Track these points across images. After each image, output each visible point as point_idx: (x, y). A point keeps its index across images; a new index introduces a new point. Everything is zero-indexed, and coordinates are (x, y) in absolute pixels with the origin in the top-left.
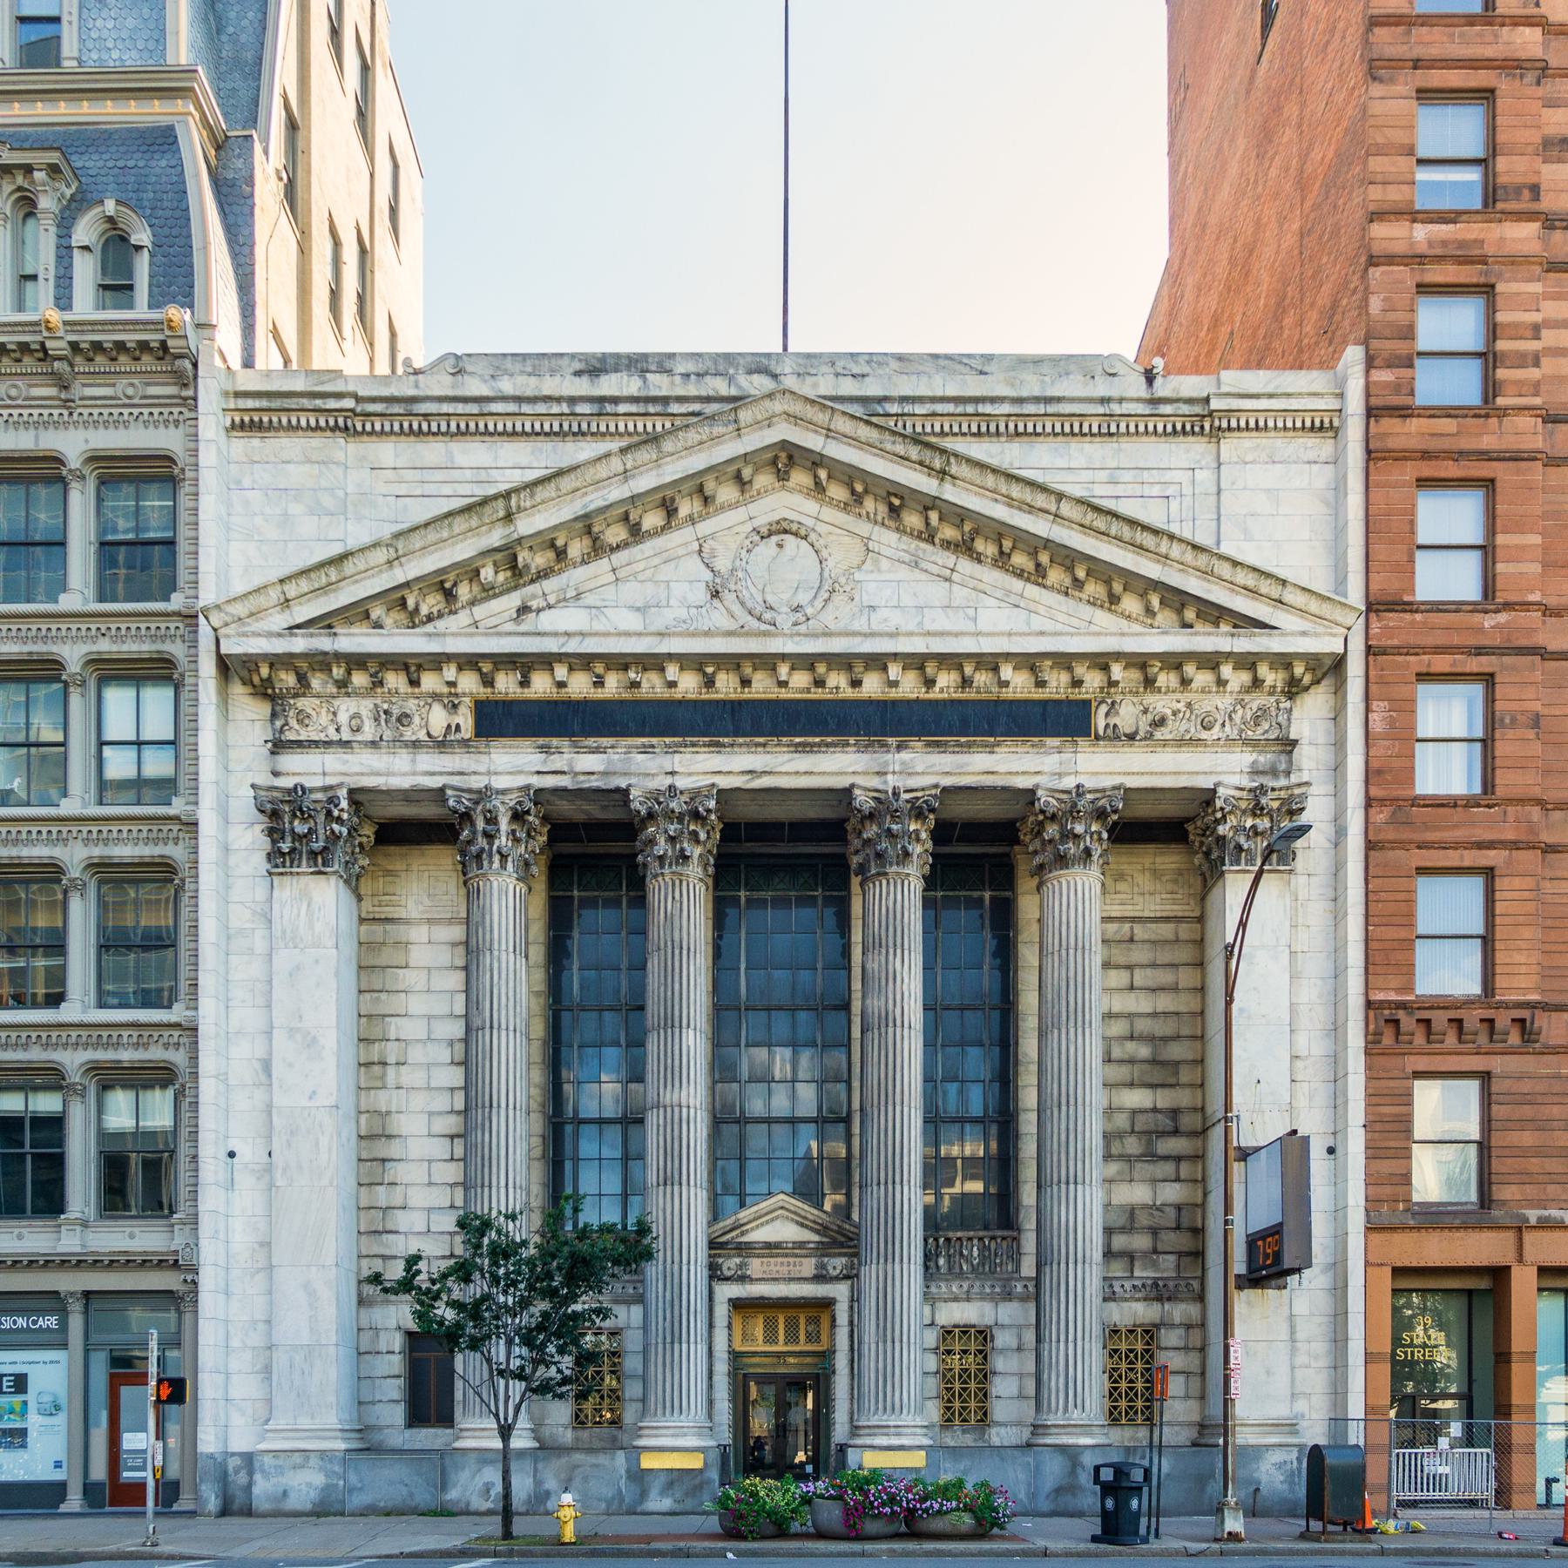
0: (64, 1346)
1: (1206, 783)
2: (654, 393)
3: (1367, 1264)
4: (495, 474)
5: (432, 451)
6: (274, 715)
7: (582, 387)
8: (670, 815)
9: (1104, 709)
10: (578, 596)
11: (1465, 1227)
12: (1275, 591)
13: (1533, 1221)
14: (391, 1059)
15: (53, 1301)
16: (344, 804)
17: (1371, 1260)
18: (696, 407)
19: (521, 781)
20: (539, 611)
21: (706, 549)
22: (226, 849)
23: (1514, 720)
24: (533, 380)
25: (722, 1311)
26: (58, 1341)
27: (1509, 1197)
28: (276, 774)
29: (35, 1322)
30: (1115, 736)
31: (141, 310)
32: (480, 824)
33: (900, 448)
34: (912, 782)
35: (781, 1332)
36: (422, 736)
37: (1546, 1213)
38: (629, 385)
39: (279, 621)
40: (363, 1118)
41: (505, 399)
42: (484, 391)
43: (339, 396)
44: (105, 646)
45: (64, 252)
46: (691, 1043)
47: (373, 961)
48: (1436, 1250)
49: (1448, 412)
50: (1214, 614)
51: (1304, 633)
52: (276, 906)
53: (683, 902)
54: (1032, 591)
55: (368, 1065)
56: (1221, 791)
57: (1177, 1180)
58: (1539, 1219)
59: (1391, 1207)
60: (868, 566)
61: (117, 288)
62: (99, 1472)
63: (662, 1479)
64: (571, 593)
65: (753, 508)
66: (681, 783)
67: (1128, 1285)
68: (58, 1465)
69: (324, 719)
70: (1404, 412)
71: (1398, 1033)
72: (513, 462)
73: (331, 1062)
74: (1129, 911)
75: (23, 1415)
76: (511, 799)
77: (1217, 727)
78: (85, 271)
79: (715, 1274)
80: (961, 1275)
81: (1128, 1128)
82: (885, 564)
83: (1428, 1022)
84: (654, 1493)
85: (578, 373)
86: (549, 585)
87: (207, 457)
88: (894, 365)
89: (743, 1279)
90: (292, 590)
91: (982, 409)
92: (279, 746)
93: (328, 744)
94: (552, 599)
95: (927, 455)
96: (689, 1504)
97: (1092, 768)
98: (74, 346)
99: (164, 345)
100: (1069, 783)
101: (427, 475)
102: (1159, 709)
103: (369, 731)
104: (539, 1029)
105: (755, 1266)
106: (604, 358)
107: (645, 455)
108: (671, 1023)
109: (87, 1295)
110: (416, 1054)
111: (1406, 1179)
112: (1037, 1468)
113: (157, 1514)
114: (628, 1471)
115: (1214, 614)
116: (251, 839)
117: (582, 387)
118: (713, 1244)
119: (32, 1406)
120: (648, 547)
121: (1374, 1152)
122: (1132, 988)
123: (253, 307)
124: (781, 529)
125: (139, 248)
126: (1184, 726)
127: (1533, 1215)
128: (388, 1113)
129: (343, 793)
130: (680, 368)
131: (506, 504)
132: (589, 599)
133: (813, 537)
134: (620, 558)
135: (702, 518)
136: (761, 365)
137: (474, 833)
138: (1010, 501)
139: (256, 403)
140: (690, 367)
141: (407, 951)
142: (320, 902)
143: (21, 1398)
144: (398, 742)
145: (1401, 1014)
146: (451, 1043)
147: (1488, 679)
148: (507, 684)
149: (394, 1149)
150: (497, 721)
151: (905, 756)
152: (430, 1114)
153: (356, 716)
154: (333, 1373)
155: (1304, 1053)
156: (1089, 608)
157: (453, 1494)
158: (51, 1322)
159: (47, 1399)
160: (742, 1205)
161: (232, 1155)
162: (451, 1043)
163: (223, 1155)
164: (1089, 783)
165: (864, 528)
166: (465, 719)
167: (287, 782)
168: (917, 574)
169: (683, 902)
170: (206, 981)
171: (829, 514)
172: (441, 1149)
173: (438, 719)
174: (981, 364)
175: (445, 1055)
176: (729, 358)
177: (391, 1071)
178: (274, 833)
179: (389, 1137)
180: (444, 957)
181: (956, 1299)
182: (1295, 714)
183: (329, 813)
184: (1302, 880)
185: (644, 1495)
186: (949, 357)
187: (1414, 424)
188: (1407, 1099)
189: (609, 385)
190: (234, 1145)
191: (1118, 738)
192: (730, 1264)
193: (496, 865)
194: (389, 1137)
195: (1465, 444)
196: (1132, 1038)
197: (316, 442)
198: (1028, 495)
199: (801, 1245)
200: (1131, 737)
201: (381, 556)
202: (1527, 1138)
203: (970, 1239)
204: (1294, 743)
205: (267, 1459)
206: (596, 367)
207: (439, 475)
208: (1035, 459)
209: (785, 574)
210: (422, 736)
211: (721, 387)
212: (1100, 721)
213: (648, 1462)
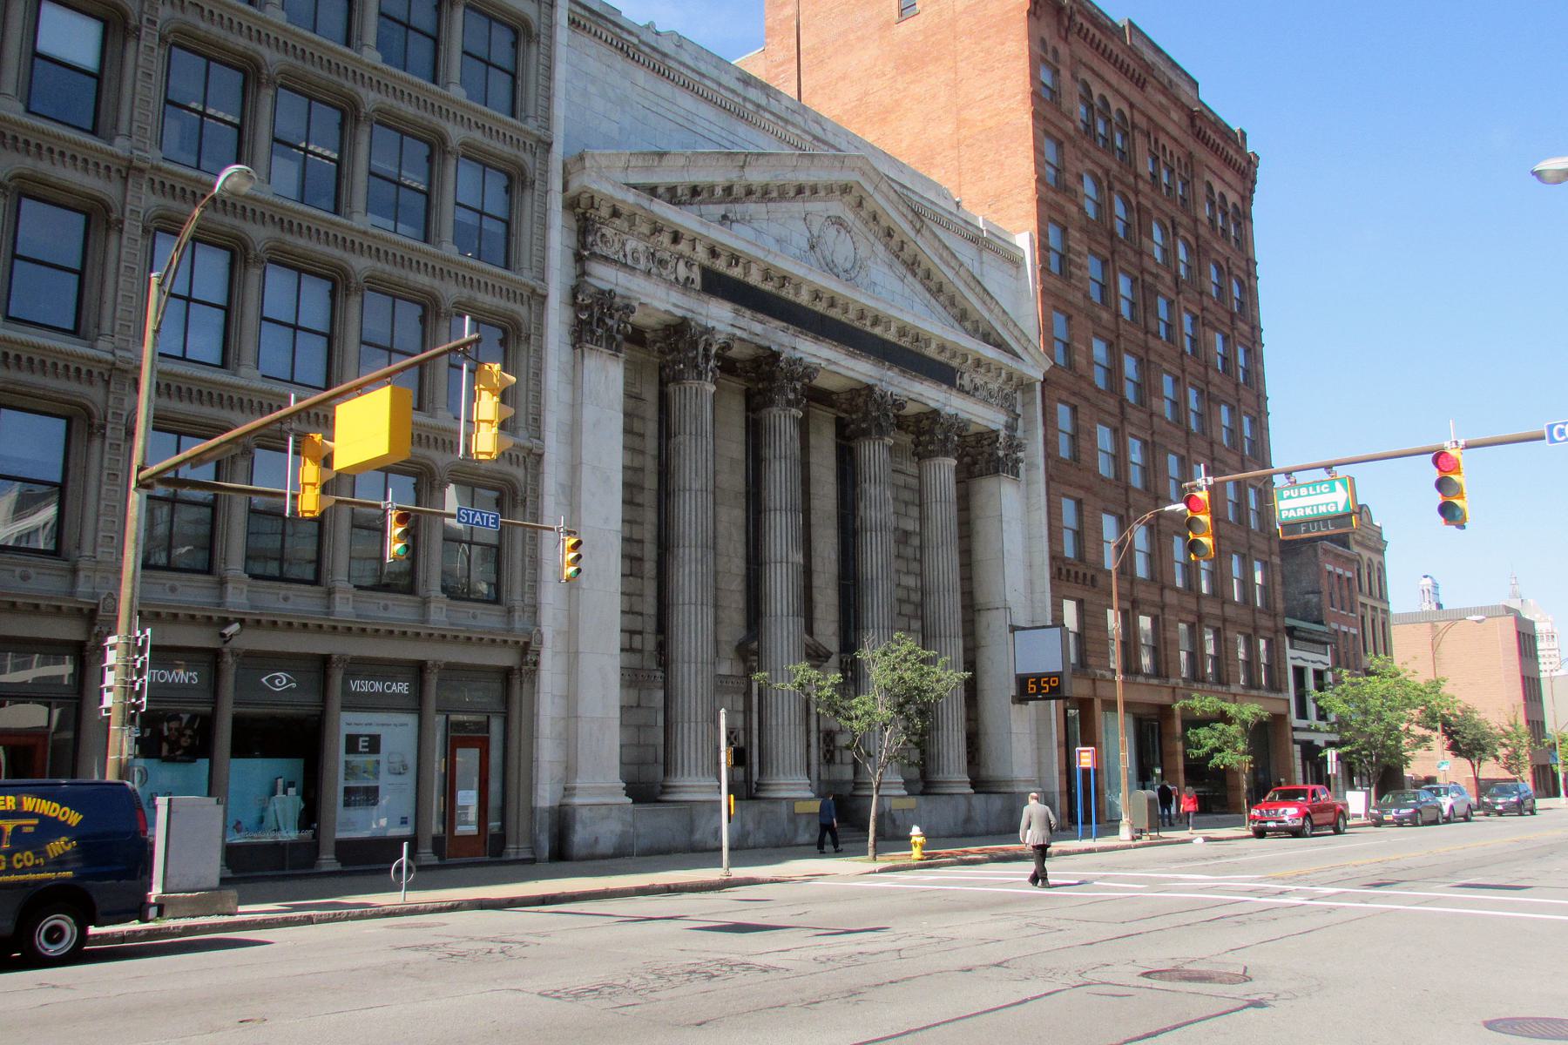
4: (697, 120)
5: (665, 88)
7: (739, 87)
29: (389, 687)
33: (905, 210)
39: (621, 178)
69: (617, 246)
75: (376, 774)
93: (616, 262)
95: (915, 220)
97: (930, 394)
101: (661, 102)
109: (451, 668)
119: (383, 767)
134: (772, 205)
138: (941, 258)
139: (583, 12)
143: (373, 757)
148: (721, 265)
150: (715, 285)
151: (890, 373)
157: (697, 836)
159: (396, 759)
173: (682, 271)
185: (796, 831)
189: (753, 94)
197: (605, 50)
201: (682, 161)
202: (468, 798)
207: (666, 105)
209: (841, 248)
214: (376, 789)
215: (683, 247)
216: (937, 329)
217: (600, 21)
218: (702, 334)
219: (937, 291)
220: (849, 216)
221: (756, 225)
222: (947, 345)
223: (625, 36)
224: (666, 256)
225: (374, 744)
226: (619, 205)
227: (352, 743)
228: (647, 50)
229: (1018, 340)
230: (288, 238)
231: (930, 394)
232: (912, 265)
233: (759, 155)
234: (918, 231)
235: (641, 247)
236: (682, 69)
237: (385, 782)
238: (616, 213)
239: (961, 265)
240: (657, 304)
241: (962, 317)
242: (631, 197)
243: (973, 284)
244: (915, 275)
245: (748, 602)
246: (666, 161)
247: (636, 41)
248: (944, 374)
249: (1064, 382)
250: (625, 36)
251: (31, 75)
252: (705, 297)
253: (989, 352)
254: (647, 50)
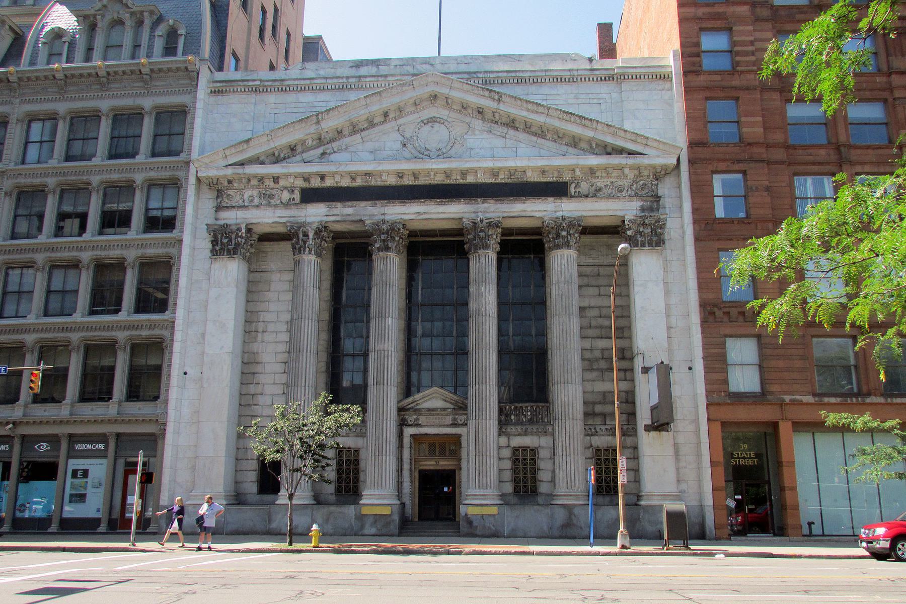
0: (106, 457)
1: (620, 214)
2: (382, 73)
3: (709, 420)
4: (316, 104)
5: (291, 97)
6: (218, 197)
7: (353, 72)
8: (381, 232)
9: (573, 185)
10: (346, 149)
11: (755, 403)
12: (644, 141)
13: (787, 401)
14: (260, 330)
15: (103, 438)
16: (244, 231)
17: (711, 417)
18: (399, 78)
19: (319, 219)
20: (330, 154)
21: (401, 129)
22: (194, 249)
23: (757, 189)
24: (333, 70)
25: (407, 440)
26: (102, 455)
27: (774, 390)
28: (216, 219)
30: (579, 196)
31: (179, 57)
32: (301, 236)
33: (481, 92)
34: (488, 215)
35: (437, 450)
36: (278, 202)
37: (793, 397)
38: (373, 70)
40: (246, 355)
41: (321, 78)
42: (313, 76)
43: (254, 80)
44: (152, 174)
45: (152, 37)
46: (390, 323)
47: (253, 291)
48: (742, 414)
49: (716, 73)
50: (620, 151)
51: (658, 156)
52: (212, 271)
53: (389, 268)
54: (540, 141)
55: (249, 332)
56: (627, 217)
57: (625, 380)
58: (791, 400)
59: (719, 394)
60: (470, 133)
61: (170, 50)
62: (116, 514)
63: (371, 519)
64: (344, 147)
65: (421, 114)
66: (387, 218)
67: (603, 428)
68: (98, 510)
69: (238, 197)
70: (697, 73)
71: (715, 317)
72: (323, 100)
73: (231, 334)
74: (597, 262)
75: (85, 489)
76: (315, 226)
77: (625, 192)
78: (159, 44)
79: (402, 423)
80: (522, 423)
81: (600, 356)
82: (477, 132)
83: (729, 313)
84: (367, 526)
85: (351, 67)
86: (335, 145)
87: (200, 105)
88: (482, 59)
89: (418, 425)
90: (228, 152)
91: (518, 74)
92: (219, 208)
94: (335, 150)
96: (384, 531)
97: (568, 208)
98: (152, 70)
99: (186, 68)
100: (559, 214)
102: (598, 184)
103: (256, 201)
104: (326, 316)
105: (422, 420)
106: (362, 61)
107: (375, 98)
108: (382, 316)
109: (118, 435)
110: (271, 328)
111: (726, 382)
112: (552, 515)
113: (137, 533)
114: (356, 515)
115: (620, 151)
116: (205, 244)
117: (353, 72)
118: (400, 410)
120: (377, 129)
121: (708, 369)
122: (600, 295)
123: (225, 47)
124: (432, 121)
125: (181, 35)
126: (610, 191)
127: (787, 398)
128: (258, 353)
129: (243, 226)
130: (393, 64)
131: (318, 117)
132: (351, 149)
133: (446, 123)
135: (399, 118)
136: (426, 61)
137: (298, 239)
138: (528, 110)
140: (398, 63)
141: (270, 285)
142: (232, 270)
143: (85, 480)
144: (269, 205)
145: (716, 310)
146: (287, 322)
147: (744, 173)
149: (259, 368)
150: (310, 196)
151: (486, 205)
152: (276, 353)
153: (252, 196)
154: (223, 469)
155: (675, 326)
156: (566, 147)
157: (274, 525)
158: (101, 446)
159: (96, 481)
160: (419, 391)
161: (185, 373)
162: (287, 322)
163: (182, 372)
164: (567, 214)
165: (468, 120)
166: (297, 196)
167: (222, 222)
168: (491, 136)
169: (389, 268)
170: (181, 302)
171: (453, 115)
172: (280, 368)
173: (286, 196)
174: (519, 58)
175: (284, 328)
176: (413, 59)
177: (260, 335)
178: (214, 242)
179: (257, 363)
180: (286, 287)
181: (520, 435)
182: (660, 186)
183: (237, 234)
184: (669, 252)
185: (362, 527)
186: (504, 56)
187: (702, 78)
188: (723, 346)
189: (363, 71)
190: (187, 369)
191: (581, 197)
192: (411, 419)
193: (307, 252)
194: (257, 363)
195: (724, 84)
196: (600, 317)
197: (243, 96)
198: (535, 108)
199: (445, 409)
200: (587, 196)
201: (266, 138)
203: (526, 407)
204: (660, 197)
205: (190, 508)
206: (359, 64)
208: (538, 94)
209: (434, 137)
210: (278, 202)
211: (409, 69)
212: (572, 190)
213: (365, 511)
214: (85, 495)
215: (282, 183)
216: (527, 159)
217: (233, 84)
218: (300, 227)
219: (541, 133)
220: (443, 113)
221: (351, 149)
222: (547, 169)
223: (251, 83)
224: (274, 192)
225: (85, 473)
226: (229, 177)
227: (75, 474)
228: (270, 83)
229: (634, 141)
230: (53, 255)
231: (568, 208)
232: (511, 124)
233: (328, 111)
234: (499, 101)
235: (255, 193)
236: (296, 82)
237: (90, 492)
238: (230, 182)
239: (549, 108)
240: (267, 221)
241: (575, 142)
242: (229, 171)
243: (567, 117)
244: (516, 129)
245: (405, 378)
246: (252, 143)
247: (258, 83)
248: (557, 189)
249: (703, 154)
250: (251, 83)
251: (866, 124)
252: (303, 206)
253: (616, 160)
254: (270, 83)
